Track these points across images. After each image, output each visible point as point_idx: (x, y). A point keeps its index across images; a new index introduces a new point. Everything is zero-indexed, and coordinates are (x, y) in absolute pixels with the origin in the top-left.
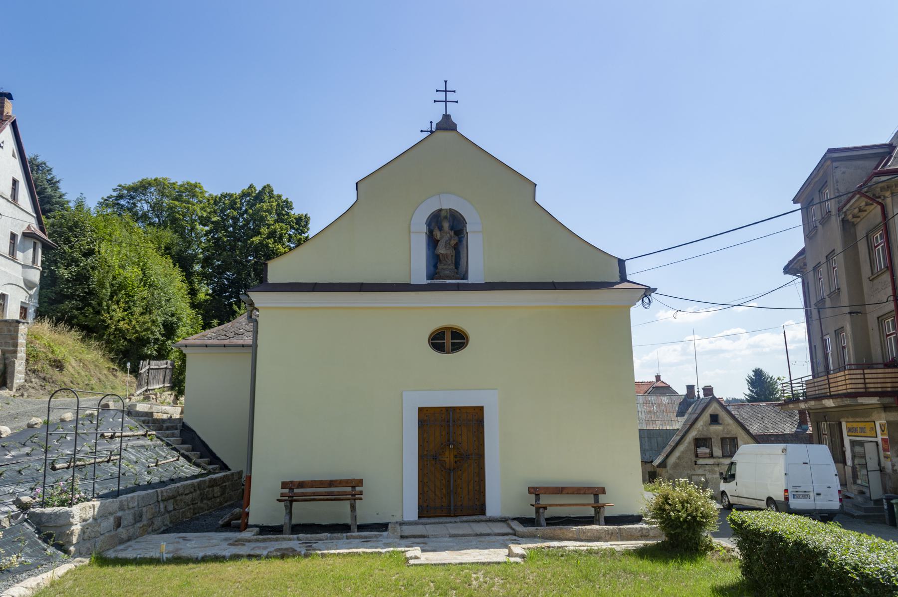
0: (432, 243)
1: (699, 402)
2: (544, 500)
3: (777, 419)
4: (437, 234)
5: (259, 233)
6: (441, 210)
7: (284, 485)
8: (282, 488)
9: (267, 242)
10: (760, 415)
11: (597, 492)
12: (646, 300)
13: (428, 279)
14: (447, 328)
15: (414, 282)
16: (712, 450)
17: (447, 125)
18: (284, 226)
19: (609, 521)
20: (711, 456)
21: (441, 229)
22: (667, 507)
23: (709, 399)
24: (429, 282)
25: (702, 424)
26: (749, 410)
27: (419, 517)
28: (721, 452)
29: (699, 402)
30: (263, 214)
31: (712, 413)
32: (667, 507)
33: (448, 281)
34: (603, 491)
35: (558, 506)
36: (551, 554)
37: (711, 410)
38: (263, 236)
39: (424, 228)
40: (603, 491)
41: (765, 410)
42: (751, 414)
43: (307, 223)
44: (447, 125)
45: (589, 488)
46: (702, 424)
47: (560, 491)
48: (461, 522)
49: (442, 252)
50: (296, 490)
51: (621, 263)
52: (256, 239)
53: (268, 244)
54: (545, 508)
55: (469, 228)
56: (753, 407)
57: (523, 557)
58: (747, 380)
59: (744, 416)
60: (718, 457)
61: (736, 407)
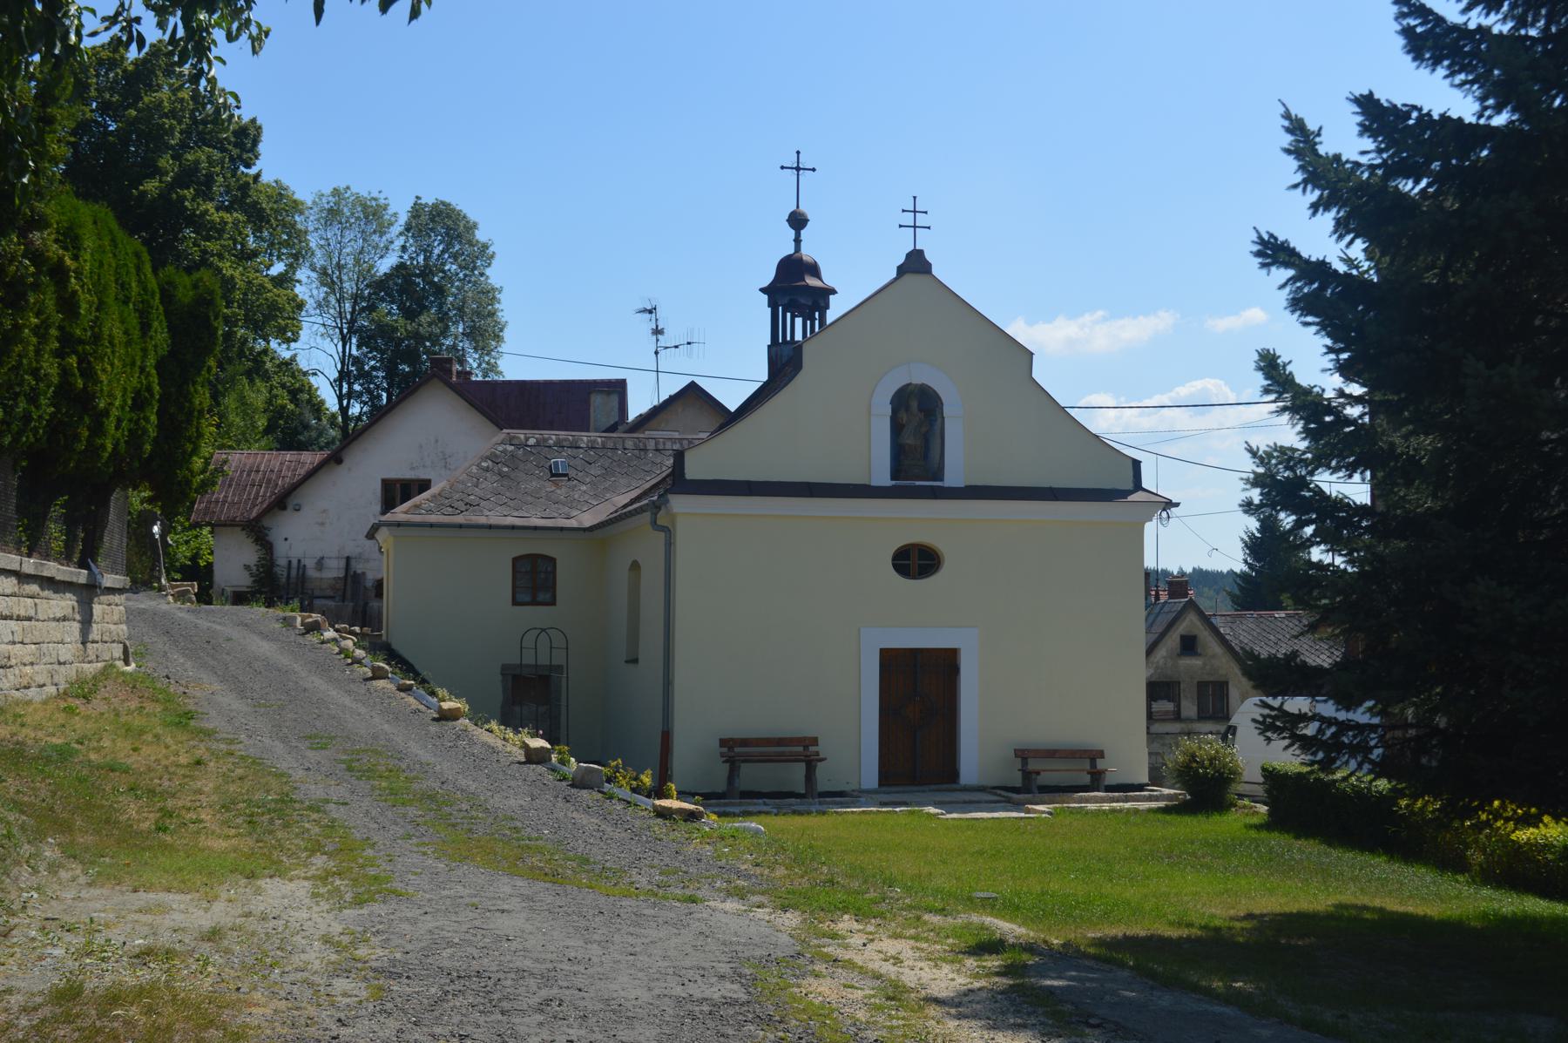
0: (897, 428)
1: (1157, 609)
2: (1033, 765)
3: (1305, 646)
4: (904, 416)
5: (158, 172)
6: (910, 384)
7: (724, 742)
8: (721, 746)
9: (178, 196)
10: (1272, 637)
11: (1094, 755)
12: (1164, 515)
13: (892, 479)
14: (914, 545)
15: (874, 483)
16: (1178, 706)
17: (916, 264)
18: (217, 155)
19: (1109, 789)
20: (1177, 717)
21: (907, 409)
22: (1194, 765)
23: (1182, 605)
24: (894, 482)
25: (1165, 654)
26: (1254, 627)
27: (880, 785)
28: (1195, 708)
29: (1157, 609)
30: (164, 123)
31: (1183, 633)
32: (1194, 765)
33: (918, 483)
34: (1101, 754)
35: (1051, 773)
36: (1072, 811)
37: (1182, 628)
38: (164, 178)
39: (888, 410)
40: (1101, 754)
41: (1284, 626)
42: (1255, 634)
43: (256, 142)
44: (916, 264)
45: (1086, 751)
46: (1165, 654)
47: (1051, 754)
48: (930, 791)
49: (909, 442)
50: (737, 750)
51: (1136, 464)
52: (151, 186)
53: (182, 199)
54: (1038, 773)
55: (947, 411)
56: (1261, 620)
57: (1050, 813)
58: (1242, 539)
59: (1241, 638)
60: (1189, 720)
61: (1228, 618)
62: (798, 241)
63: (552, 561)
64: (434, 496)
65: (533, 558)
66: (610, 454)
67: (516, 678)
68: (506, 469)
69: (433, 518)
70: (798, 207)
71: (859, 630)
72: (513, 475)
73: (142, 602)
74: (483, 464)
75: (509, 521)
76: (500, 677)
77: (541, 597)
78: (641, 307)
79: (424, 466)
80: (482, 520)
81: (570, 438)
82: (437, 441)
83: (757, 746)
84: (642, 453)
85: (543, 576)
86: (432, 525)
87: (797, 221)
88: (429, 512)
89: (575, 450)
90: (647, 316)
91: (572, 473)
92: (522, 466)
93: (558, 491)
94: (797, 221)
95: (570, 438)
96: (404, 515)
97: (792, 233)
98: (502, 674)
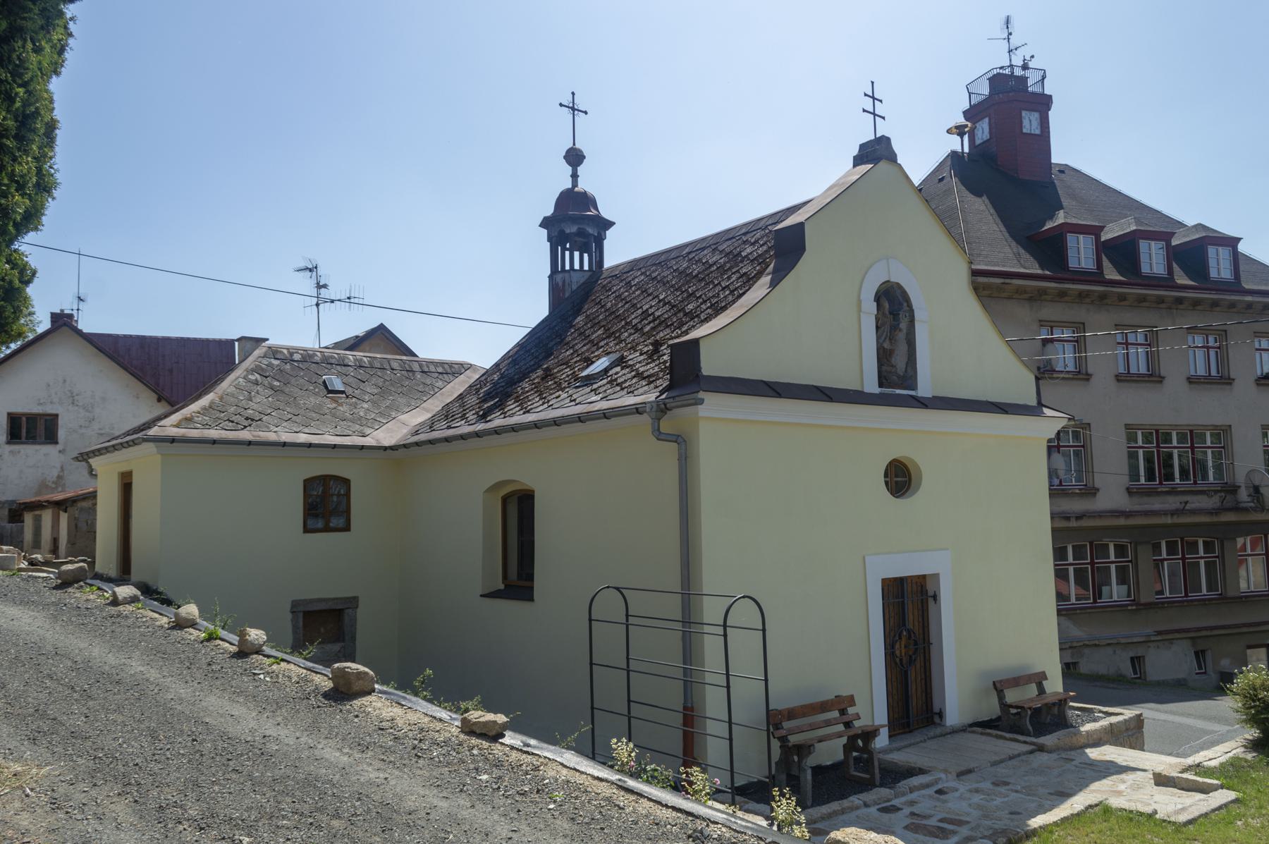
33: (898, 391)
62: (575, 176)
63: (346, 482)
64: (204, 409)
65: (325, 480)
66: (379, 374)
67: (307, 614)
68: (276, 383)
69: (214, 433)
70: (574, 144)
71: (864, 558)
72: (287, 390)
73: (1002, 802)
74: (250, 377)
75: (302, 438)
76: (289, 616)
77: (335, 522)
78: (302, 265)
79: (51, 403)
80: (272, 437)
81: (336, 356)
82: (65, 381)
83: (804, 715)
84: (411, 374)
85: (335, 499)
86: (214, 442)
87: (574, 158)
88: (206, 426)
89: (343, 368)
90: (309, 274)
91: (349, 391)
92: (293, 381)
93: (340, 408)
94: (574, 158)
95: (336, 356)
96: (176, 430)
97: (569, 170)
98: (293, 612)
